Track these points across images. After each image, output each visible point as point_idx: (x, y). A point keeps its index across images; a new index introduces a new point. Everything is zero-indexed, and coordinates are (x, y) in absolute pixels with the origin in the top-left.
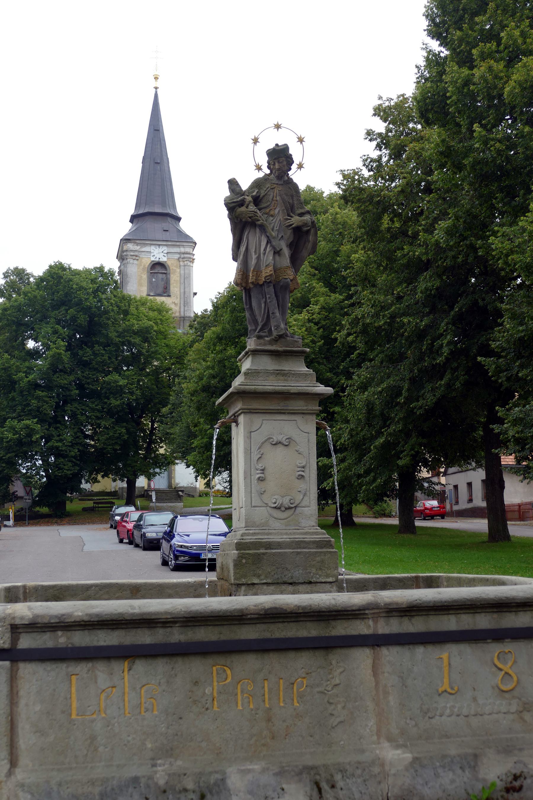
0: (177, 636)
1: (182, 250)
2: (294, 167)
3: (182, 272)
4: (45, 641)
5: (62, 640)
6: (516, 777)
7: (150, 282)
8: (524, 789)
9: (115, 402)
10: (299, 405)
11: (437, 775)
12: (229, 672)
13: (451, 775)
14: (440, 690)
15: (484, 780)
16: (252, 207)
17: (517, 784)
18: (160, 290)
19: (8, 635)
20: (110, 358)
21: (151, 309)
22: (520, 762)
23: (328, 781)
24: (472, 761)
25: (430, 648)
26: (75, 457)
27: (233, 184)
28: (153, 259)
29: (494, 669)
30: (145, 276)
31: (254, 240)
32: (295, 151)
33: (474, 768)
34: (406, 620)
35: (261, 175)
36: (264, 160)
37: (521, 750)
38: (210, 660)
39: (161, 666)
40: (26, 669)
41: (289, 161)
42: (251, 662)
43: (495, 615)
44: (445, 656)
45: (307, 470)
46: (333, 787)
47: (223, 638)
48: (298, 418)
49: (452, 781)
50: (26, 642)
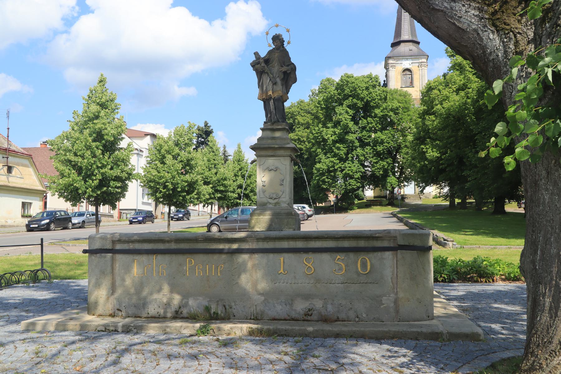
0: (173, 246)
1: (420, 61)
2: (285, 44)
3: (421, 73)
4: (125, 246)
5: (131, 246)
6: (309, 310)
7: (402, 80)
8: (313, 315)
9: (380, 148)
10: (281, 152)
11: (274, 307)
12: (193, 261)
13: (281, 307)
14: (279, 272)
15: (295, 310)
16: (263, 64)
17: (310, 313)
18: (408, 84)
19: (111, 244)
20: (376, 124)
21: (400, 95)
22: (312, 304)
23: (229, 306)
24: (290, 301)
25: (276, 255)
26: (358, 178)
27: (256, 54)
28: (404, 67)
29: (304, 265)
30: (399, 77)
31: (266, 80)
32: (286, 38)
33: (291, 305)
34: (265, 243)
35: (271, 48)
36: (271, 41)
37: (312, 299)
38: (185, 256)
39: (167, 257)
40: (118, 257)
41: (282, 41)
42: (201, 257)
43: (305, 242)
44: (282, 259)
45: (285, 181)
46: (231, 308)
47: (191, 248)
48: (282, 159)
49: (281, 310)
50: (118, 247)
